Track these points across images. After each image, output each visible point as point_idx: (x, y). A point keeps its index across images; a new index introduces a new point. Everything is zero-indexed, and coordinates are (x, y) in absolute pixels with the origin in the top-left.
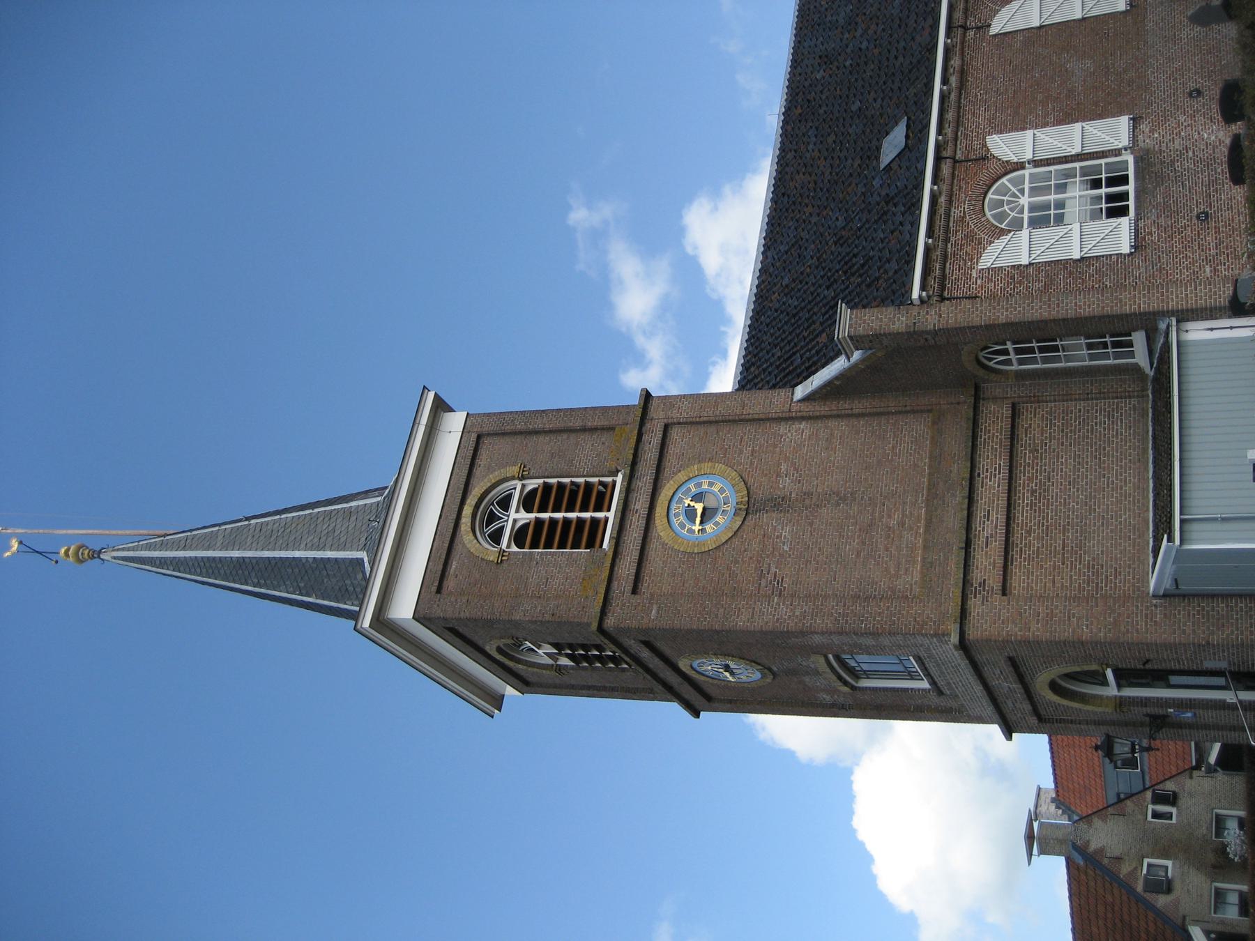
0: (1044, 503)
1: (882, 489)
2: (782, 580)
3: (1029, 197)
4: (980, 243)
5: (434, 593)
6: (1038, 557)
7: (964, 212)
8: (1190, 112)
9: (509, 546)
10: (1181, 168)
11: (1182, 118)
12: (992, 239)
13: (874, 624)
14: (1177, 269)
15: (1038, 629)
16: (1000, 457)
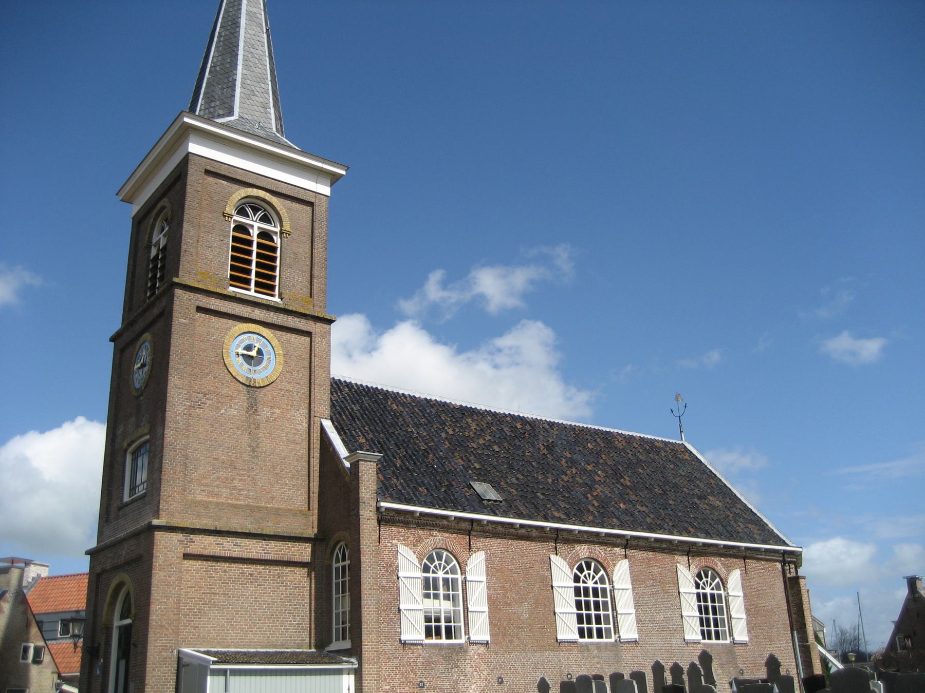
6: (208, 577)
9: (235, 221)
11: (485, 673)
16: (276, 554)
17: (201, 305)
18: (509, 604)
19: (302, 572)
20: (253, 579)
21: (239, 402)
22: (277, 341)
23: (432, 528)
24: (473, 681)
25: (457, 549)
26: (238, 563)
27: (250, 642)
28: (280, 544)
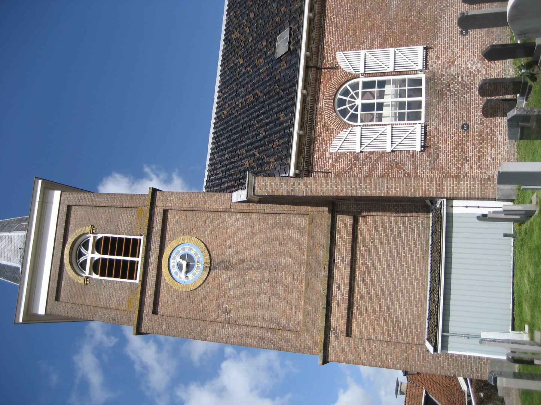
0: (370, 280)
1: (281, 261)
2: (230, 312)
3: (362, 99)
4: (331, 133)
5: (54, 300)
6: (366, 313)
7: (322, 108)
8: (461, 46)
9: (90, 274)
10: (454, 89)
11: (456, 50)
12: (339, 130)
13: (278, 346)
14: (448, 165)
15: (365, 359)
16: (346, 251)
17: (151, 310)
18: (387, 22)
19: (363, 224)
20: (368, 271)
21: (223, 277)
22: (173, 242)
23: (315, 112)
24: (464, 66)
25: (334, 82)
26: (354, 285)
27: (422, 276)
28: (338, 246)
